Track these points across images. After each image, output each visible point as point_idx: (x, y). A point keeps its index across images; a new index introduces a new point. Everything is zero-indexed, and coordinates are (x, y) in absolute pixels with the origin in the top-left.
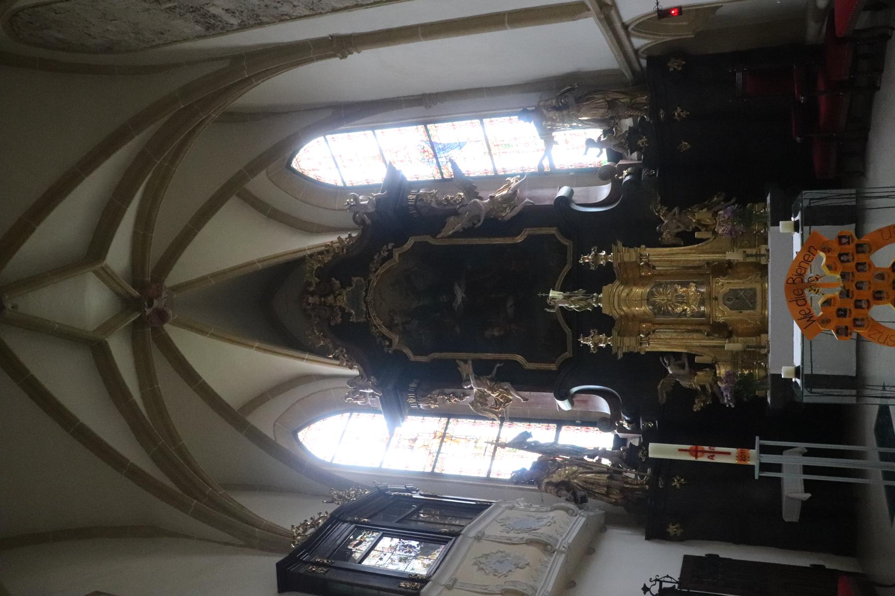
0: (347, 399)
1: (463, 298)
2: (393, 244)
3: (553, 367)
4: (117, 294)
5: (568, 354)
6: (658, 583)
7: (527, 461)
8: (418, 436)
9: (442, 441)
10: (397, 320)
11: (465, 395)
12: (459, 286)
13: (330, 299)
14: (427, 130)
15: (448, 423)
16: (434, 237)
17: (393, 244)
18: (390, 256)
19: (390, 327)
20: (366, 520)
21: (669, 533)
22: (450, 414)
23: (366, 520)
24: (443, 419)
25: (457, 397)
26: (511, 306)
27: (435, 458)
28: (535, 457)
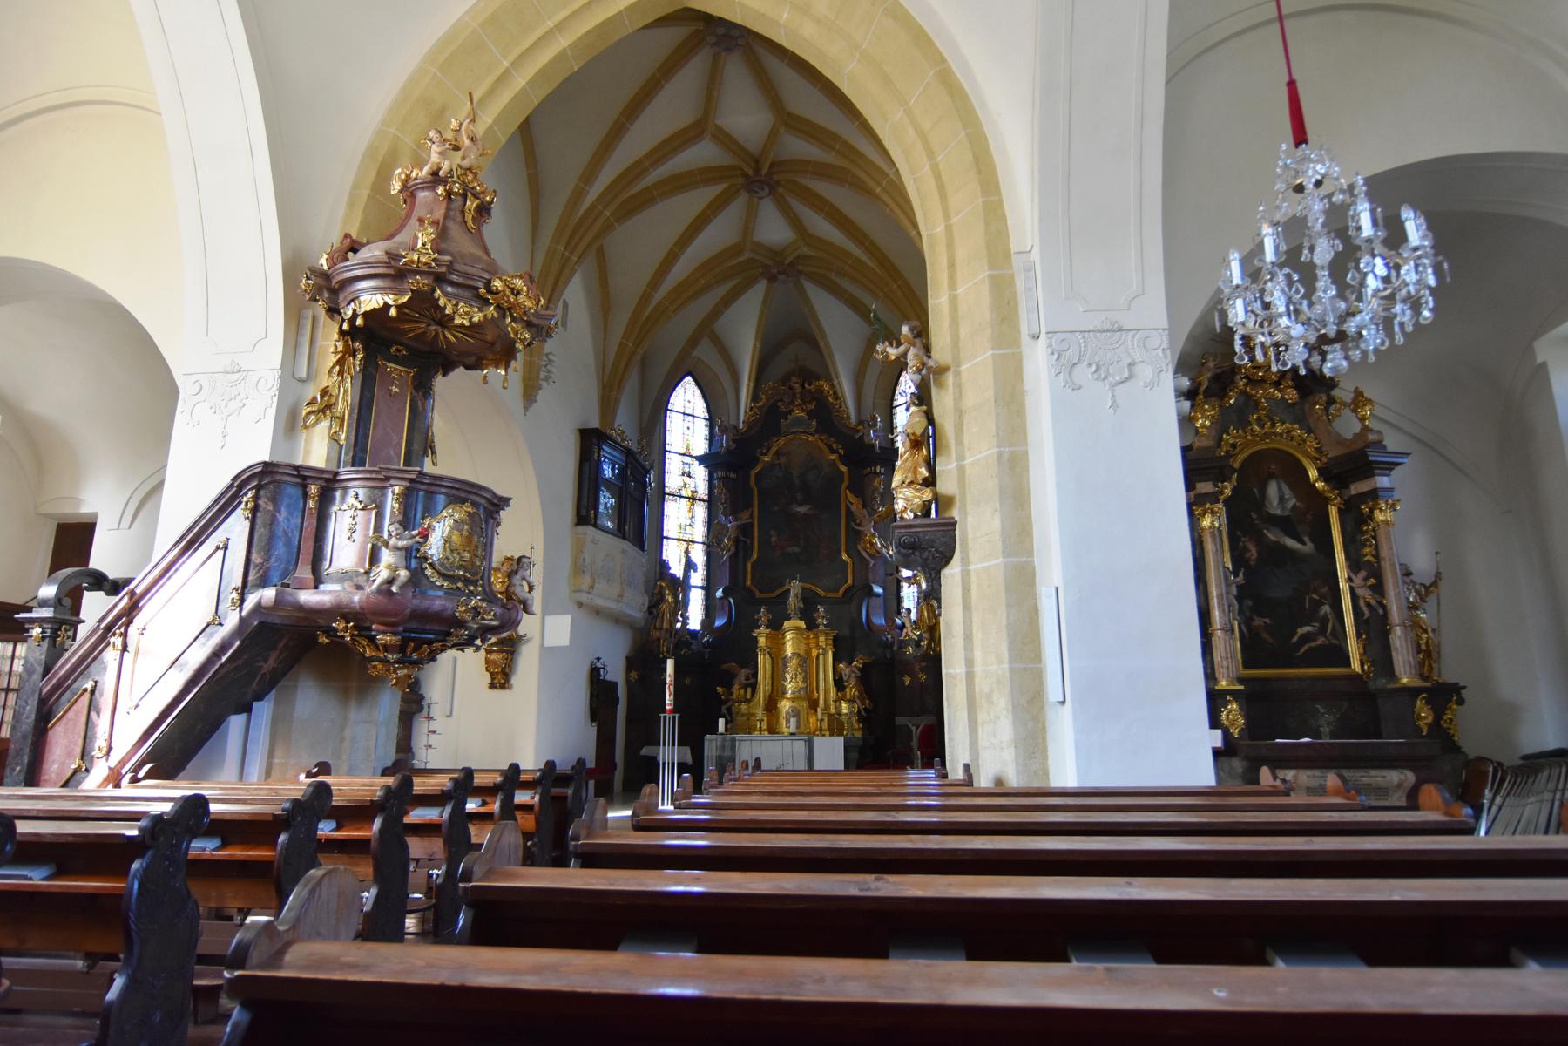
1: (799, 512)
3: (749, 583)
5: (758, 595)
7: (677, 569)
10: (783, 459)
13: (798, 402)
15: (704, 501)
16: (847, 488)
18: (833, 451)
19: (777, 454)
22: (711, 503)
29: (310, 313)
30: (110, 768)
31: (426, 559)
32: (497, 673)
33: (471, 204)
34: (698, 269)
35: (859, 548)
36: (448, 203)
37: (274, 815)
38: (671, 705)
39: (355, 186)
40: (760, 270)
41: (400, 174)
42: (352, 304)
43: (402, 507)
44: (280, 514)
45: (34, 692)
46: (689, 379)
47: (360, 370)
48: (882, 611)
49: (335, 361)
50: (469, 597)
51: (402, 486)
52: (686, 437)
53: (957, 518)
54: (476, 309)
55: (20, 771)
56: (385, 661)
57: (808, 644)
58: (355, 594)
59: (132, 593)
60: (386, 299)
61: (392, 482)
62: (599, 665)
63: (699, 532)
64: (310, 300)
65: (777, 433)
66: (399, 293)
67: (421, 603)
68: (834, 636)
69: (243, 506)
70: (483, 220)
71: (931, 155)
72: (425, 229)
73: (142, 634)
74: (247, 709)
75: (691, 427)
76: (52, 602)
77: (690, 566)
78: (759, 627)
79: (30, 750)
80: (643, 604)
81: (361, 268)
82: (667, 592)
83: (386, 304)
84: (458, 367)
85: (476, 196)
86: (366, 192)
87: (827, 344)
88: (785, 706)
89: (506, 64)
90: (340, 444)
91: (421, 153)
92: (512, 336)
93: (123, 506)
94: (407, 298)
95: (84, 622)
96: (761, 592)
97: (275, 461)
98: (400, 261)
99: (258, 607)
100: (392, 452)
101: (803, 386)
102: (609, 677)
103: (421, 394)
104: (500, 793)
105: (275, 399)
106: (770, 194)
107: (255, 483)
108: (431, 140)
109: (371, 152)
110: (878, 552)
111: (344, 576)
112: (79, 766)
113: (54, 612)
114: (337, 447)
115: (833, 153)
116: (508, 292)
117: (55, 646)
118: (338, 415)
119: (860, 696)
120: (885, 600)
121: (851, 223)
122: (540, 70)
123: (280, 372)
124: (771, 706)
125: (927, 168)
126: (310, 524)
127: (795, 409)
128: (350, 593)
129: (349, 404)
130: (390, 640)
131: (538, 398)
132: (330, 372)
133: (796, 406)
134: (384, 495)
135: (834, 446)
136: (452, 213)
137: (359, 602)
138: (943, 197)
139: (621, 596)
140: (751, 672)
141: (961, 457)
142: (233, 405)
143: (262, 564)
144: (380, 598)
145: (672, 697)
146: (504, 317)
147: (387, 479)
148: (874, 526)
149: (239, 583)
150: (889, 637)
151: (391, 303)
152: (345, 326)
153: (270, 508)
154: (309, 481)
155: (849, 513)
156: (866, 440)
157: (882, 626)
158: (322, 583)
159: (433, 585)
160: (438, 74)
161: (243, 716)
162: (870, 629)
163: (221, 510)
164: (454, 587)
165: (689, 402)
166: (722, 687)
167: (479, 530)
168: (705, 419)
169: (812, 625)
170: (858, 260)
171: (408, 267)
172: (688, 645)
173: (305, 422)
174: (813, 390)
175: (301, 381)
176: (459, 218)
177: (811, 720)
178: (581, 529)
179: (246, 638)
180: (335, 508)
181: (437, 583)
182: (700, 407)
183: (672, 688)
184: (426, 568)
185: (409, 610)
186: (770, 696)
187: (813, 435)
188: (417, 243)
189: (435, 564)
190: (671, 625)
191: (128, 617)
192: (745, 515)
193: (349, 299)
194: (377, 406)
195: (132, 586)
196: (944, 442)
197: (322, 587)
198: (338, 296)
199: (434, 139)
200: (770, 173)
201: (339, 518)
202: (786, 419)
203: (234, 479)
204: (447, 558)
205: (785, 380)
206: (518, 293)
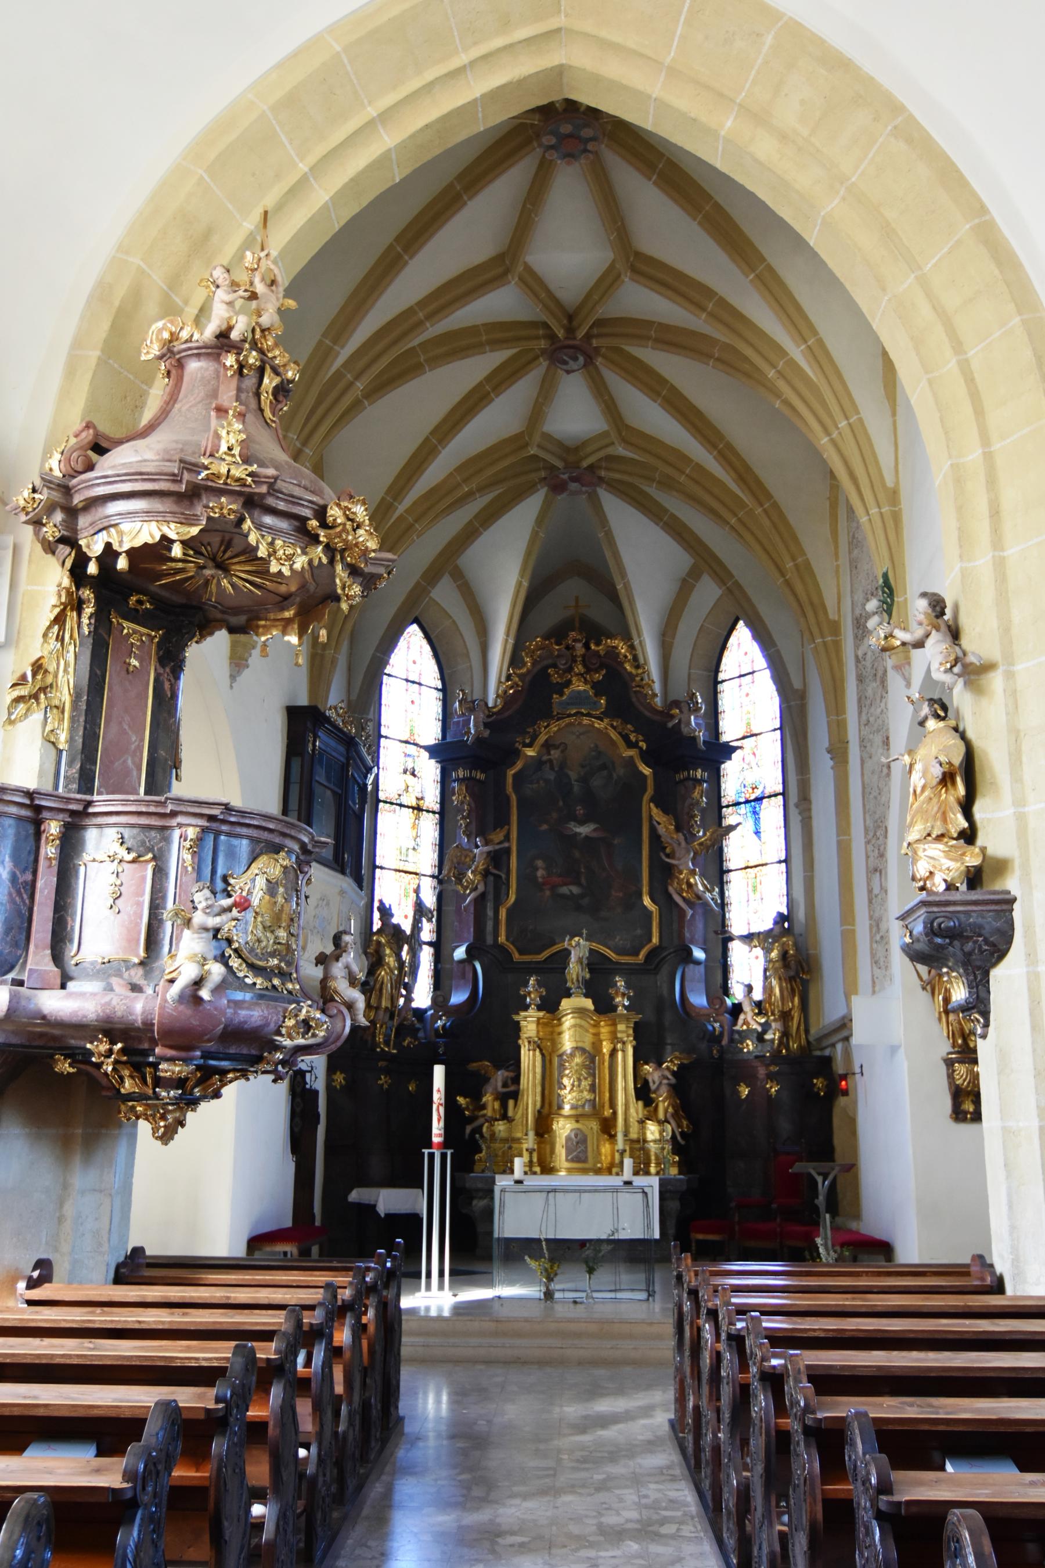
1: (580, 834)
2: (644, 748)
4: (585, 444)
5: (516, 956)
7: (404, 919)
9: (413, 808)
10: (555, 754)
11: (468, 836)
12: (595, 830)
13: (579, 668)
14: (776, 795)
15: (434, 812)
16: (652, 800)
17: (644, 748)
18: (630, 745)
19: (547, 746)
21: (335, 1074)
22: (444, 814)
24: (438, 806)
25: (466, 827)
26: (571, 891)
28: (407, 927)
31: (229, 941)
33: (269, 382)
34: (459, 469)
35: (671, 889)
36: (239, 381)
37: (208, 1411)
38: (440, 1135)
39: (77, 344)
40: (543, 474)
41: (160, 331)
43: (196, 860)
46: (414, 628)
47: (90, 632)
48: (702, 986)
51: (197, 826)
53: (1015, 892)
54: (299, 551)
57: (597, 1035)
61: (180, 819)
63: (427, 859)
65: (547, 714)
66: (189, 521)
67: (235, 1013)
68: (636, 1023)
70: (280, 406)
71: (958, 347)
72: (230, 424)
77: (420, 909)
78: (526, 1008)
81: (129, 480)
82: (388, 951)
83: (164, 537)
85: (276, 371)
86: (94, 355)
87: (627, 587)
88: (563, 1128)
89: (303, 167)
91: (173, 296)
96: (521, 953)
98: (199, 473)
100: (130, 762)
101: (587, 646)
103: (168, 670)
104: (349, 1315)
106: (585, 366)
108: (214, 283)
109: (101, 293)
110: (699, 897)
111: (107, 969)
114: (54, 752)
115: (704, 316)
118: (56, 702)
119: (675, 1115)
120: (706, 967)
121: (698, 413)
122: (352, 180)
124: (543, 1127)
125: (952, 364)
127: (574, 679)
128: (126, 997)
130: (180, 1072)
131: (250, 661)
132: (45, 635)
133: (577, 675)
134: (167, 840)
135: (633, 737)
137: (143, 1013)
138: (979, 412)
140: (512, 1074)
141: (1019, 802)
144: (182, 1008)
145: (442, 1124)
146: (332, 561)
147: (174, 814)
148: (693, 860)
150: (717, 1025)
151: (173, 536)
152: (92, 569)
154: (45, 814)
155: (655, 837)
156: (685, 730)
157: (703, 1008)
158: (71, 979)
162: (687, 1013)
166: (465, 1097)
168: (436, 689)
169: (604, 1007)
170: (699, 468)
171: (210, 484)
172: (413, 1031)
174: (602, 653)
177: (603, 1151)
182: (429, 672)
183: (442, 1110)
184: (230, 956)
185: (222, 1026)
186: (539, 1112)
187: (602, 720)
192: (498, 836)
193: (101, 526)
196: (989, 777)
197: (70, 985)
198: (77, 518)
199: (219, 282)
200: (588, 336)
202: (561, 694)
204: (259, 941)
205: (558, 634)
206: (359, 527)
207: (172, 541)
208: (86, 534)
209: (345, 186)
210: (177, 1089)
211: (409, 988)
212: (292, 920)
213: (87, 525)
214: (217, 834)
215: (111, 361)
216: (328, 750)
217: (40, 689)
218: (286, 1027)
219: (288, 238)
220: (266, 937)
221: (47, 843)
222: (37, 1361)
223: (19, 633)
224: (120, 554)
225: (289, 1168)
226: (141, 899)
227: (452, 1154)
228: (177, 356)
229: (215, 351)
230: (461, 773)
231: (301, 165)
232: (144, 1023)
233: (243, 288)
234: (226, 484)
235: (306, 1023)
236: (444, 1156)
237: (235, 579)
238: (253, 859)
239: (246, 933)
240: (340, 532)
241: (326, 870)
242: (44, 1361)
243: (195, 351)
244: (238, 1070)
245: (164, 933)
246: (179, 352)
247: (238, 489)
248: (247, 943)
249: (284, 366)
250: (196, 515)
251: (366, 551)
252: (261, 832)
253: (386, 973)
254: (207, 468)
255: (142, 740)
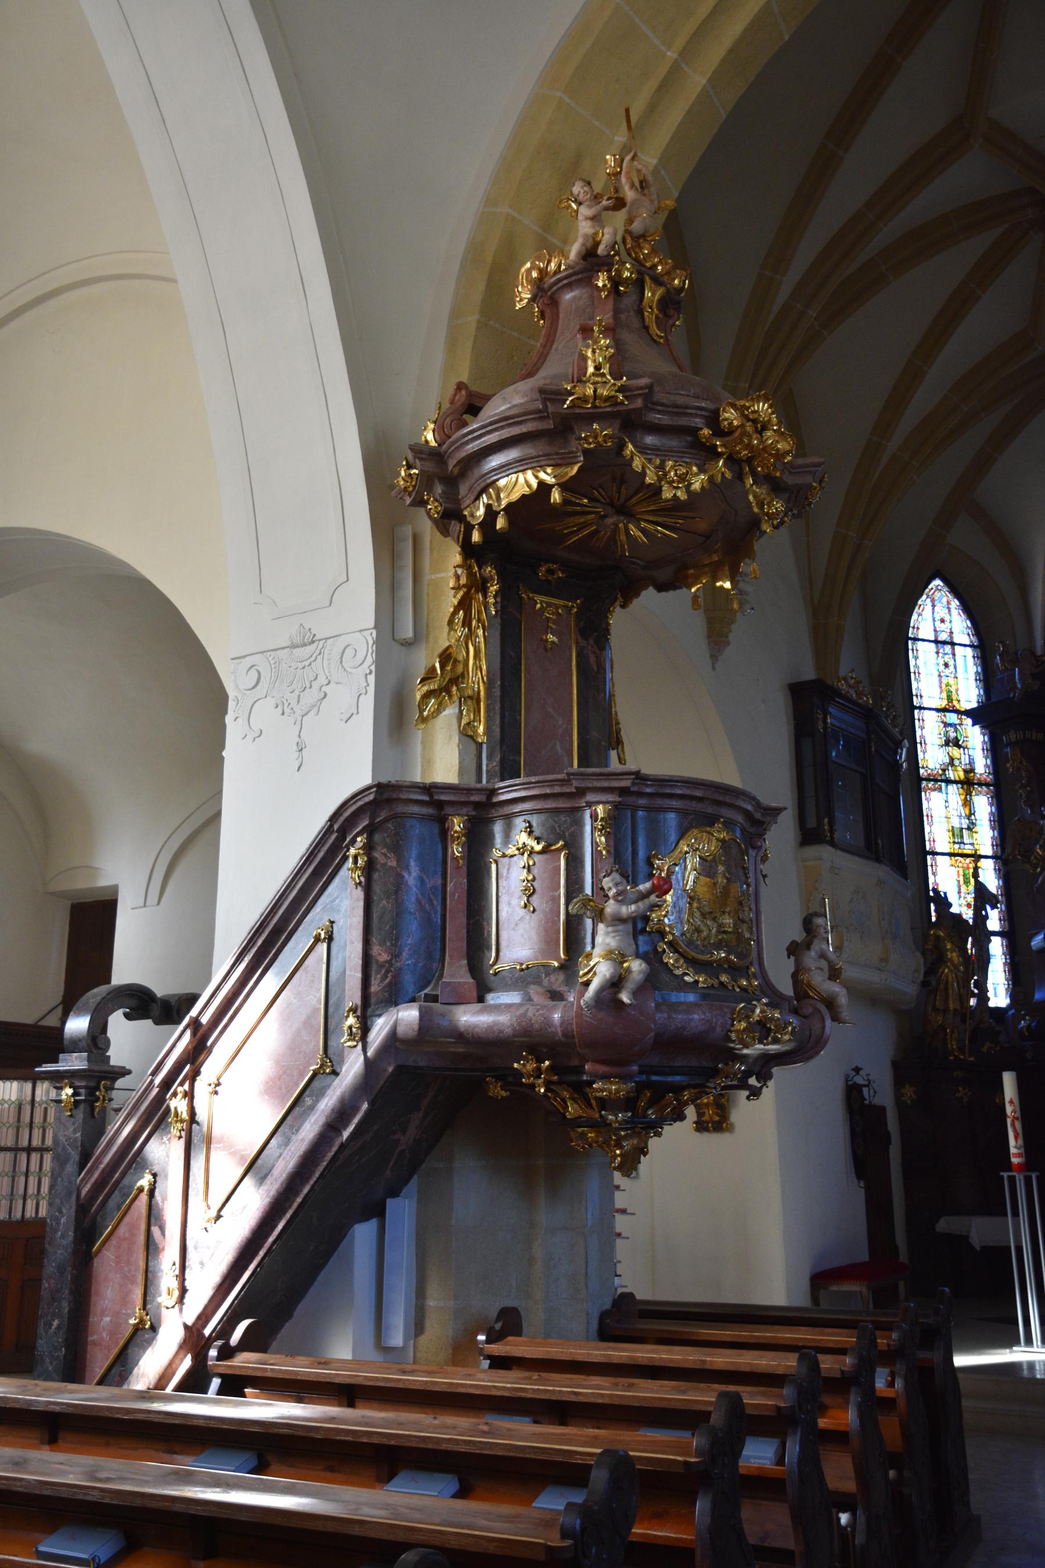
0: (1000, 645)
6: (866, 1083)
7: (961, 906)
8: (964, 749)
11: (1031, 807)
15: (987, 785)
20: (873, 749)
23: (873, 749)
27: (939, 778)
28: (968, 915)
29: (408, 531)
30: (186, 1326)
31: (662, 934)
32: (707, 1105)
38: (1019, 1155)
39: (456, 313)
41: (529, 271)
42: (485, 498)
43: (612, 843)
44: (410, 874)
45: (69, 1194)
46: (937, 582)
49: (456, 602)
50: (749, 1002)
52: (945, 680)
54: (695, 469)
55: (59, 1327)
56: (600, 1126)
58: (553, 1009)
59: (195, 1023)
60: (542, 475)
61: (590, 797)
62: (859, 1080)
64: (411, 505)
69: (350, 863)
70: (671, 322)
72: (596, 342)
73: (216, 1093)
74: (378, 1211)
75: (951, 663)
76: (84, 1044)
77: (982, 897)
79: (71, 1292)
80: (916, 971)
81: (496, 430)
83: (541, 484)
84: (646, 588)
85: (657, 281)
86: (472, 319)
89: (672, 55)
90: (476, 742)
92: (756, 510)
93: (147, 876)
94: (576, 468)
95: (124, 1072)
97: (383, 780)
99: (393, 1038)
102: (877, 1101)
103: (591, 641)
104: (853, 1390)
105: (372, 679)
107: (366, 822)
109: (474, 252)
112: (142, 1321)
113: (89, 1060)
114: (473, 746)
116: (749, 428)
117: (93, 1116)
118: (470, 692)
122: (731, 51)
123: (374, 632)
126: (457, 885)
128: (543, 1007)
129: (484, 673)
130: (618, 1091)
131: (731, 637)
132: (451, 622)
134: (579, 824)
136: (623, 317)
137: (562, 1023)
139: (884, 960)
142: (310, 697)
143: (390, 962)
144: (601, 1015)
145: (1020, 1141)
146: (740, 477)
147: (581, 792)
149: (358, 1000)
151: (549, 480)
152: (476, 537)
153: (393, 863)
154: (448, 810)
158: (490, 990)
159: (682, 986)
160: (566, 99)
161: (372, 1225)
163: (317, 874)
164: (716, 982)
165: (942, 621)
167: (741, 872)
171: (577, 411)
173: (421, 711)
175: (407, 644)
176: (635, 323)
178: (813, 851)
179: (376, 1097)
180: (496, 853)
181: (686, 978)
182: (960, 627)
183: (1018, 1125)
185: (652, 1034)
188: (586, 368)
189: (677, 944)
190: (962, 1004)
191: (192, 1063)
193: (479, 489)
194: (527, 671)
195: (194, 1012)
197: (492, 998)
198: (458, 488)
199: (581, 197)
201: (504, 871)
203: (333, 819)
204: (698, 930)
206: (765, 427)
207: (550, 487)
208: (468, 502)
209: (724, 62)
210: (626, 1111)
211: (982, 985)
212: (740, 903)
213: (467, 492)
214: (635, 808)
215: (491, 322)
216: (843, 726)
217: (450, 680)
218: (737, 1031)
219: (667, 140)
220: (708, 927)
221: (453, 842)
222: (422, 1446)
223: (427, 626)
224: (499, 513)
225: (859, 1195)
226: (556, 894)
227: (1037, 1177)
228: (549, 293)
229: (585, 275)
230: (1013, 736)
231: (669, 53)
232: (565, 1035)
233: (605, 198)
234: (594, 407)
235: (762, 1023)
236: (1028, 1181)
237: (643, 524)
238: (682, 836)
239: (682, 923)
240: (741, 437)
241: (856, 859)
242: (430, 1446)
243: (565, 282)
244: (694, 1087)
245: (585, 930)
246: (550, 288)
247: (609, 409)
248: (683, 934)
249: (668, 273)
250: (572, 452)
251: (780, 455)
252: (688, 802)
253: (950, 970)
254: (571, 394)
255: (571, 721)
